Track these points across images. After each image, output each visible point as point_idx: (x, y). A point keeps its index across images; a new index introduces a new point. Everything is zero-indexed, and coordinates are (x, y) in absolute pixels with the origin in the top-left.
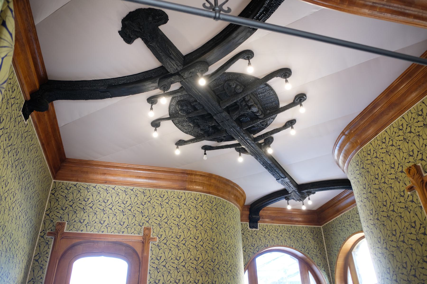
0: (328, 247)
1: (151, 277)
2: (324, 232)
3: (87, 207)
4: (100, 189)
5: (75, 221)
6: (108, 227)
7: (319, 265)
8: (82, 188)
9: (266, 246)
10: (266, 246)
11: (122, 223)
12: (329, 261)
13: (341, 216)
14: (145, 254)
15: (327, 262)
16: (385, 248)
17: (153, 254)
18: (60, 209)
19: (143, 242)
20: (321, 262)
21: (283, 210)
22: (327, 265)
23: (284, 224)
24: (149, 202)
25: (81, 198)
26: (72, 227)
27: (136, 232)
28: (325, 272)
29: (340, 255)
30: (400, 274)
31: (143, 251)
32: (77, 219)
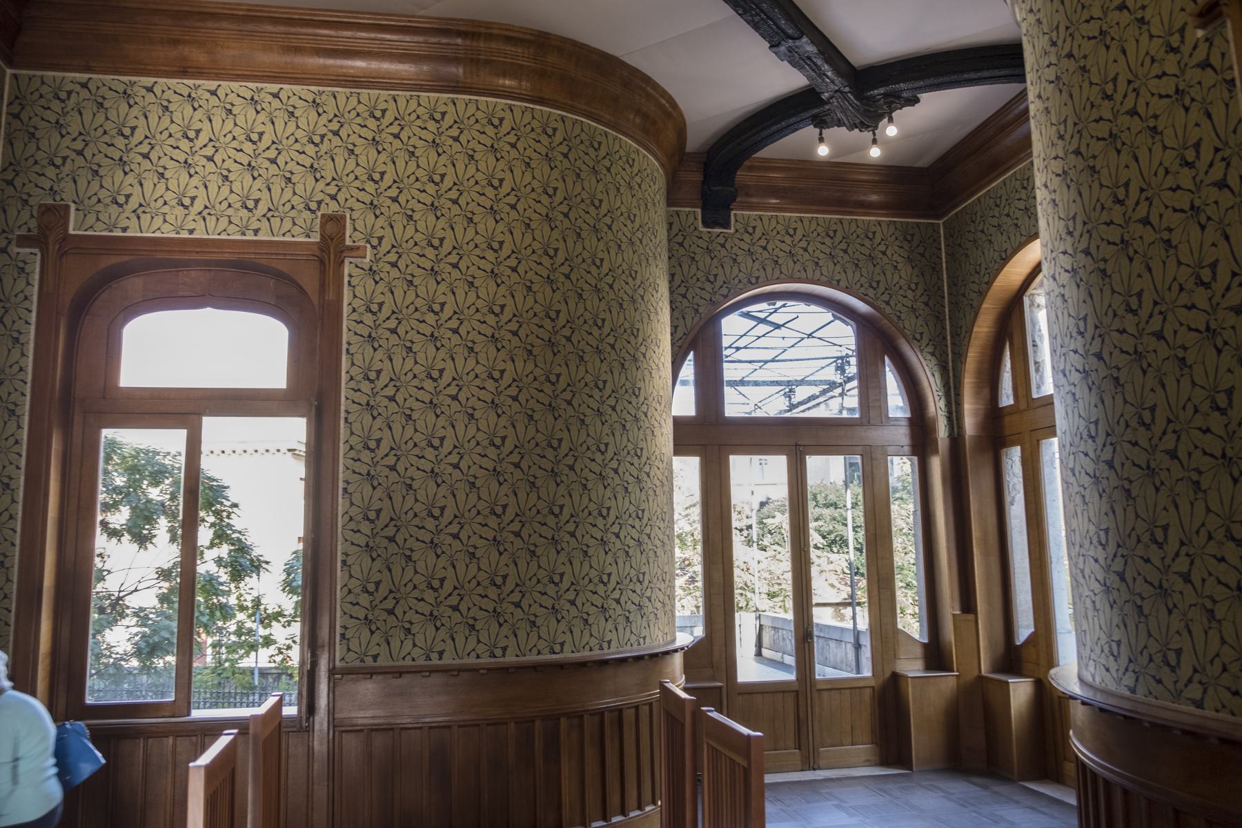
0: (953, 284)
1: (353, 364)
2: (946, 238)
3: (132, 155)
4: (169, 94)
5: (99, 201)
6: (208, 218)
7: (918, 336)
8: (109, 94)
9: (753, 280)
10: (753, 280)
11: (251, 204)
12: (951, 326)
13: (1004, 182)
14: (331, 296)
15: (944, 328)
16: (1082, 251)
17: (355, 296)
18: (45, 162)
19: (322, 262)
20: (925, 329)
21: (807, 168)
22: (945, 338)
23: (817, 212)
24: (336, 133)
25: (108, 126)
26: (91, 219)
27: (297, 230)
28: (933, 360)
29: (984, 306)
30: (1115, 334)
31: (323, 287)
32: (103, 194)
